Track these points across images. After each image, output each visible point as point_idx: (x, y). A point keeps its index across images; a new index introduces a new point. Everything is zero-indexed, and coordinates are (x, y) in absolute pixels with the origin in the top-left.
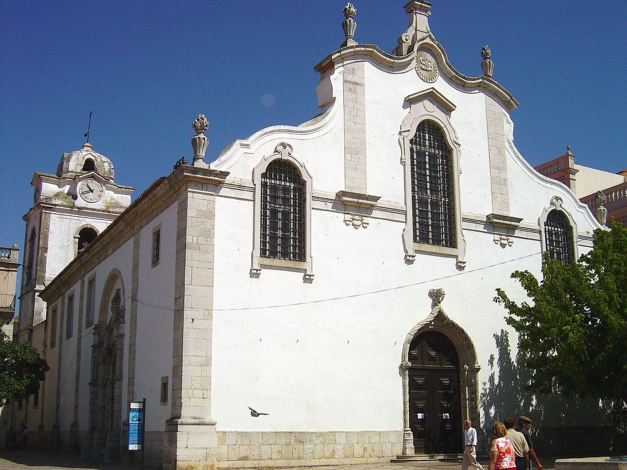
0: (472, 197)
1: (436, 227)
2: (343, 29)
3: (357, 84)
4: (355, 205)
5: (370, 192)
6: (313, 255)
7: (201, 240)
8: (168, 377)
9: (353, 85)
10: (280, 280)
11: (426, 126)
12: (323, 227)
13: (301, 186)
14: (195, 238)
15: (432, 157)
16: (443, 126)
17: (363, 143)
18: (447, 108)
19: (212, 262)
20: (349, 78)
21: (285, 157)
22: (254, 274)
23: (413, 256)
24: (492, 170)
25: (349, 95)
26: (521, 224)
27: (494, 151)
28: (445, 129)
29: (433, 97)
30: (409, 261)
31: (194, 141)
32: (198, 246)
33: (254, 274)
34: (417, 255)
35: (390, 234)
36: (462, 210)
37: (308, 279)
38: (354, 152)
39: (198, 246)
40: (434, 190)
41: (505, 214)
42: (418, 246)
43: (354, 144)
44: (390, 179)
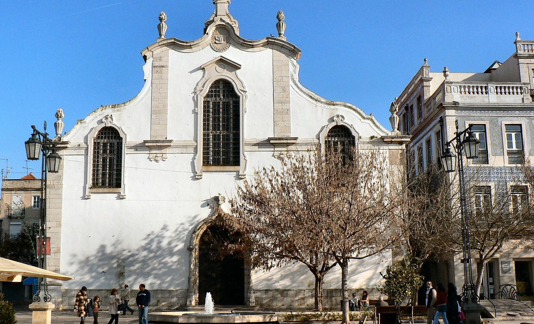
0: (254, 125)
1: (226, 153)
2: (288, 145)
3: (163, 67)
4: (155, 146)
6: (125, 183)
7: (55, 183)
9: (159, 68)
10: (105, 199)
11: (221, 86)
12: (131, 162)
13: (115, 141)
14: (52, 182)
15: (223, 108)
16: (231, 81)
17: (165, 106)
18: (234, 67)
19: (61, 195)
20: (157, 64)
23: (200, 176)
25: (156, 75)
28: (233, 83)
29: (223, 62)
30: (196, 177)
31: (55, 124)
32: (53, 187)
33: (121, 198)
35: (180, 163)
36: (245, 137)
38: (158, 112)
39: (53, 187)
41: (285, 135)
42: (205, 168)
43: (158, 107)
44: (185, 124)
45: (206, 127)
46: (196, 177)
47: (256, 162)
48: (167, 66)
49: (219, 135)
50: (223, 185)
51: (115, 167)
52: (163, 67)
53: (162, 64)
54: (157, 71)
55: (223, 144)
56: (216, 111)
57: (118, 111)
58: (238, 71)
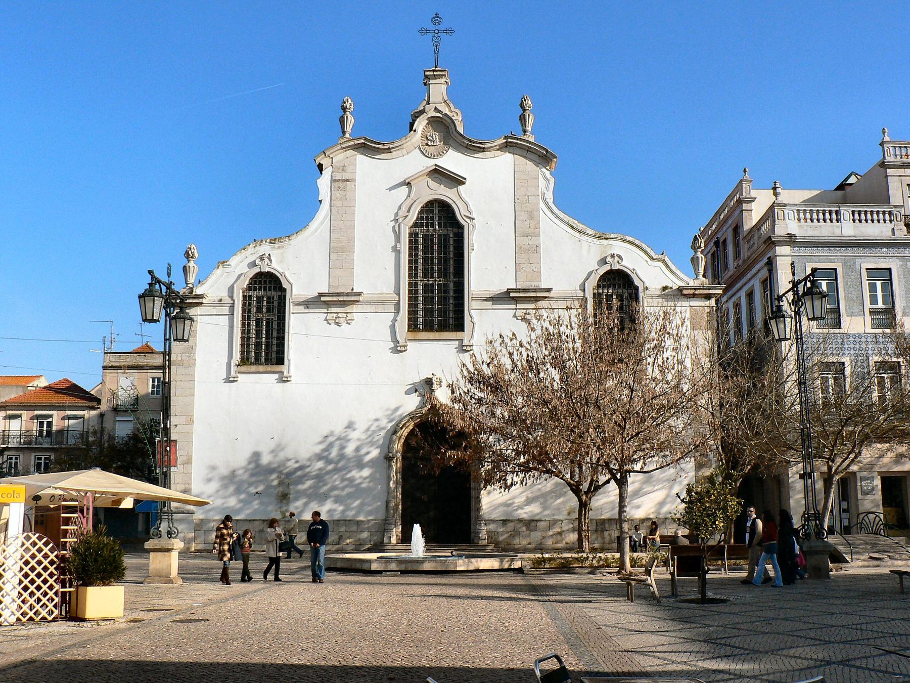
3: (348, 180)
4: (335, 302)
5: (544, 286)
7: (184, 357)
8: (165, 485)
9: (342, 183)
12: (300, 326)
17: (351, 240)
18: (455, 181)
19: (193, 375)
20: (338, 176)
21: (267, 269)
22: (229, 380)
24: (333, 256)
26: (552, 294)
27: (523, 216)
28: (454, 206)
29: (439, 174)
30: (398, 349)
32: (181, 363)
33: (229, 380)
34: (409, 343)
36: (472, 288)
37: (283, 380)
38: (340, 250)
40: (443, 273)
42: (411, 335)
44: (381, 267)
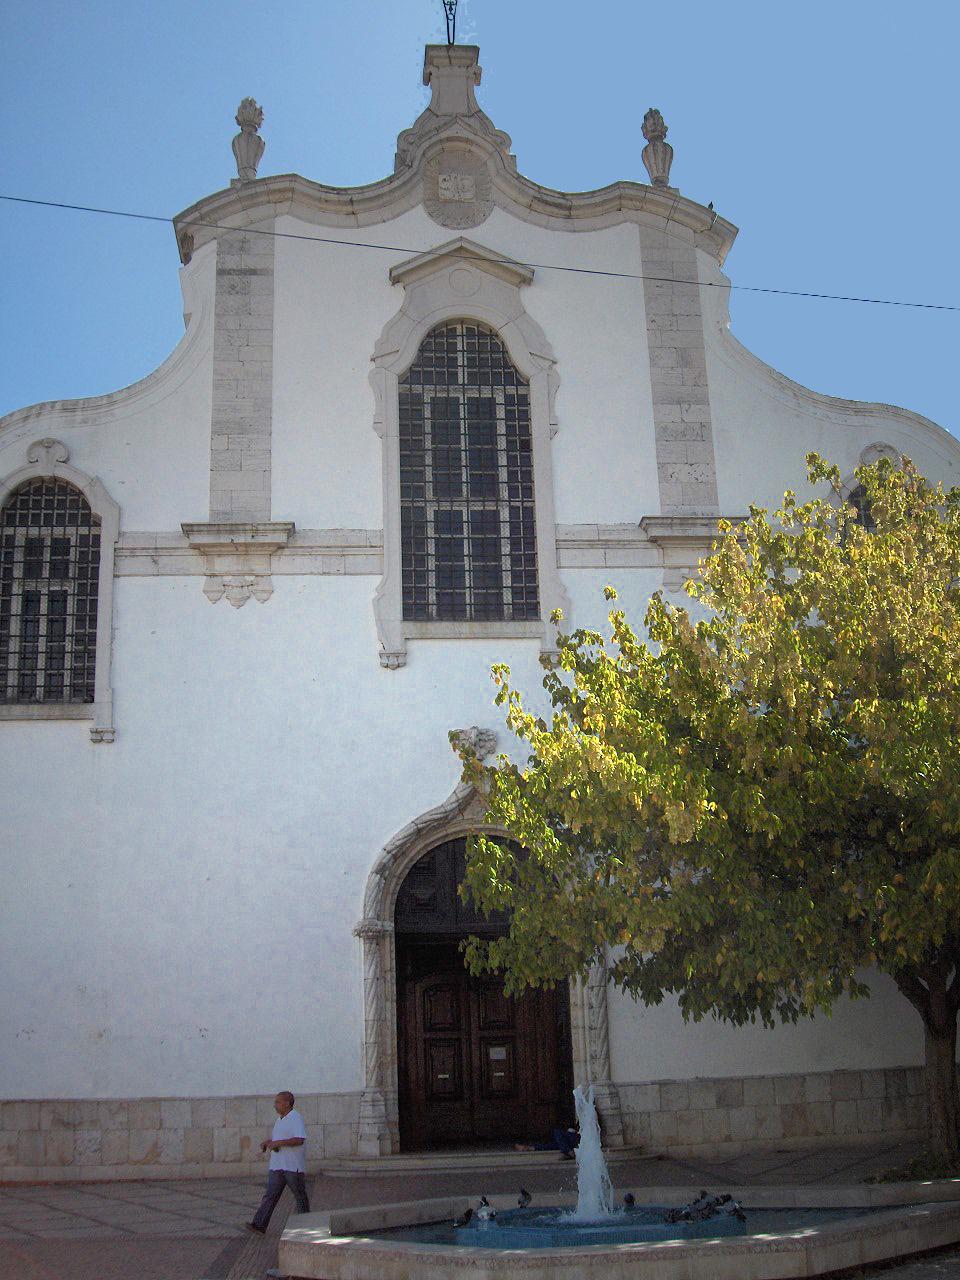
3: (253, 272)
20: (232, 262)
35: (348, 606)
42: (412, 627)
44: (342, 469)
45: (410, 486)
46: (395, 660)
47: (602, 599)
48: (267, 272)
49: (53, 575)
50: (481, 679)
51: (70, 626)
52: (253, 272)
53: (249, 262)
54: (233, 287)
55: (467, 551)
56: (445, 432)
57: (85, 422)
58: (527, 295)
